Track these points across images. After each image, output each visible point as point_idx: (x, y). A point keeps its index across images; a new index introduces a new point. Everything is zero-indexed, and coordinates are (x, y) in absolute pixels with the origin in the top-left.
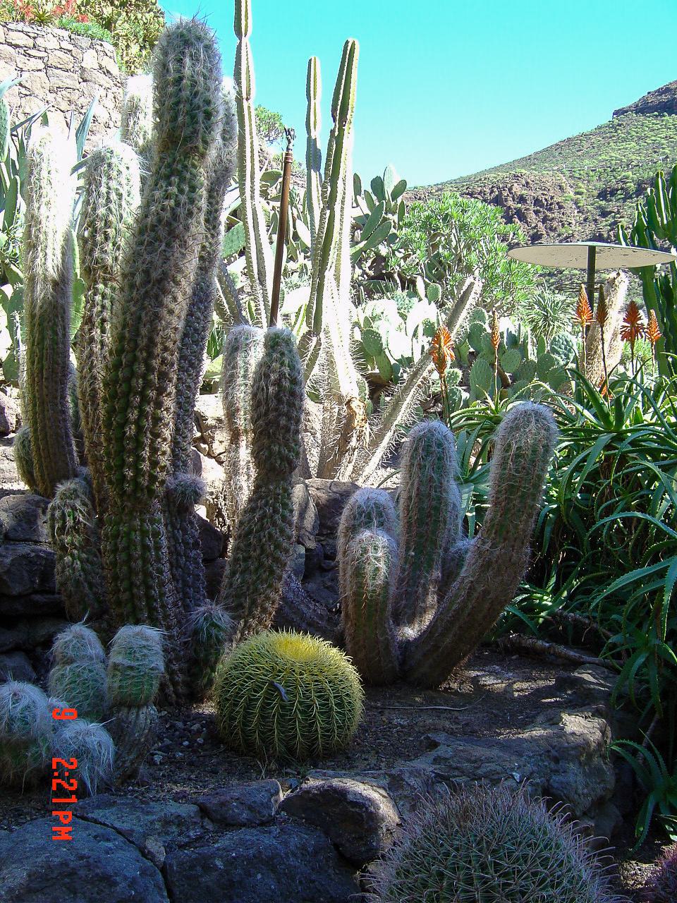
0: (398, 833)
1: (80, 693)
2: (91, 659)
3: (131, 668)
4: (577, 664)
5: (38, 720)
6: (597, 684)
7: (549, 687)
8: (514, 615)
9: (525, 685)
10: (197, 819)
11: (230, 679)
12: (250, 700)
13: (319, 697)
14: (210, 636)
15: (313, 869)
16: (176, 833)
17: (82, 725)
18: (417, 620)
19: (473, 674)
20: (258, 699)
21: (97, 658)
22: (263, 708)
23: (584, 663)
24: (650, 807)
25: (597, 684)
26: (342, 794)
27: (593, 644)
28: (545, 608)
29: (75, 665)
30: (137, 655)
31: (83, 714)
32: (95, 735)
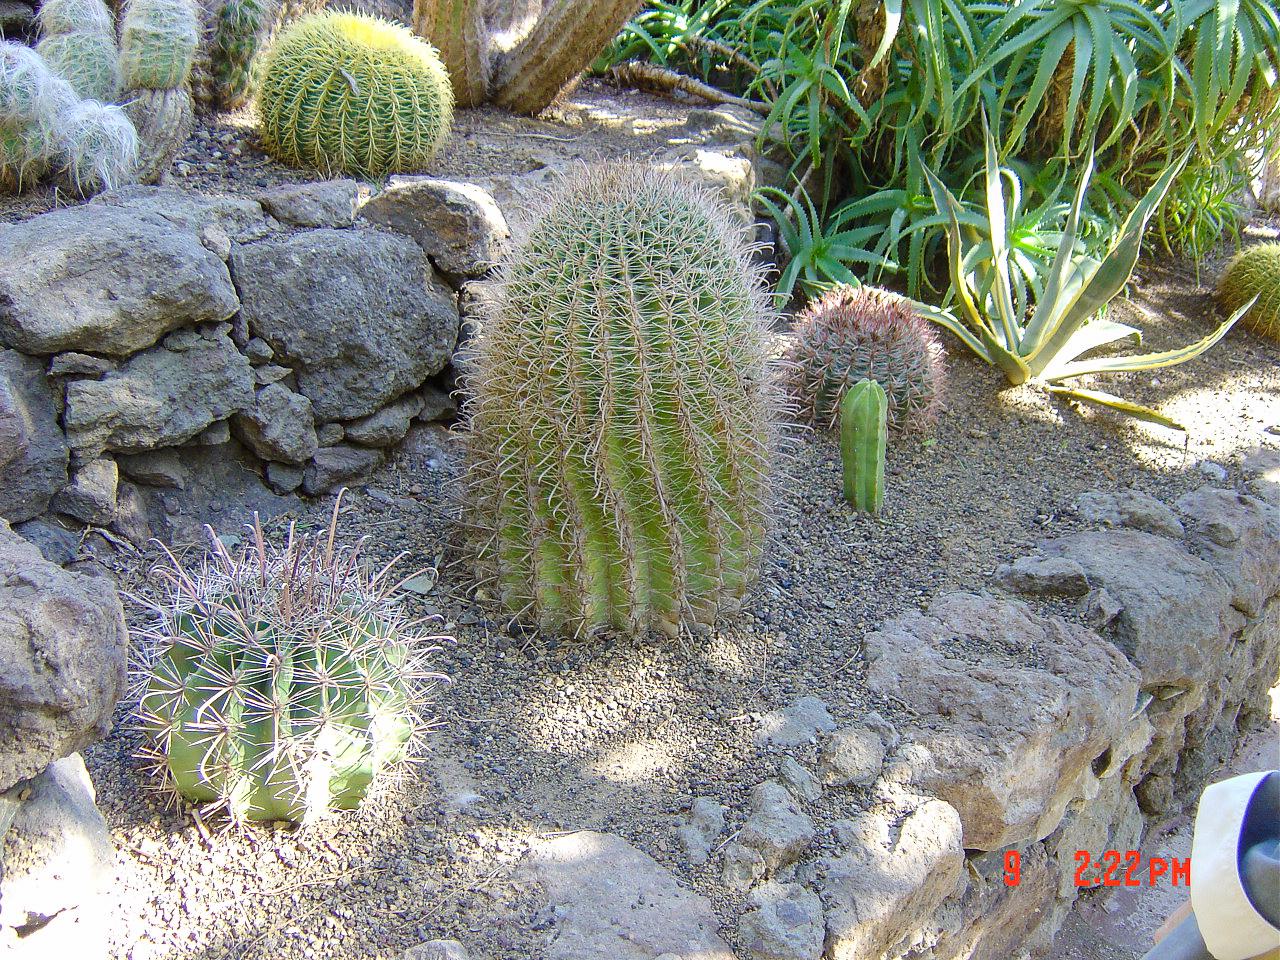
0: (506, 247)
1: (83, 72)
2: (96, 28)
3: (157, 36)
4: (714, 103)
5: (41, 93)
6: (740, 125)
7: (680, 127)
8: (638, 38)
9: (648, 123)
10: (260, 217)
11: (280, 68)
12: (309, 93)
13: (399, 94)
14: (244, 20)
15: (406, 279)
16: (235, 231)
17: (93, 107)
18: (514, 25)
19: (581, 106)
20: (320, 93)
21: (104, 27)
22: (326, 104)
23: (723, 103)
24: (795, 270)
25: (740, 125)
26: (441, 195)
27: (736, 80)
28: (674, 32)
29: (74, 35)
30: (164, 19)
31: (84, 95)
32: (115, 121)
